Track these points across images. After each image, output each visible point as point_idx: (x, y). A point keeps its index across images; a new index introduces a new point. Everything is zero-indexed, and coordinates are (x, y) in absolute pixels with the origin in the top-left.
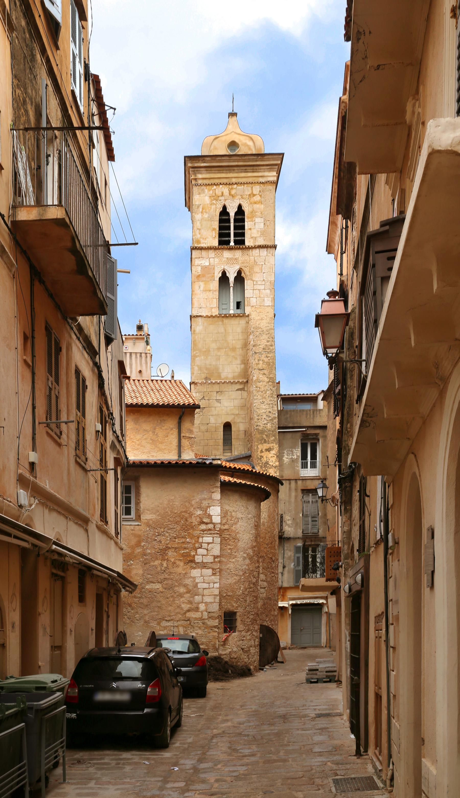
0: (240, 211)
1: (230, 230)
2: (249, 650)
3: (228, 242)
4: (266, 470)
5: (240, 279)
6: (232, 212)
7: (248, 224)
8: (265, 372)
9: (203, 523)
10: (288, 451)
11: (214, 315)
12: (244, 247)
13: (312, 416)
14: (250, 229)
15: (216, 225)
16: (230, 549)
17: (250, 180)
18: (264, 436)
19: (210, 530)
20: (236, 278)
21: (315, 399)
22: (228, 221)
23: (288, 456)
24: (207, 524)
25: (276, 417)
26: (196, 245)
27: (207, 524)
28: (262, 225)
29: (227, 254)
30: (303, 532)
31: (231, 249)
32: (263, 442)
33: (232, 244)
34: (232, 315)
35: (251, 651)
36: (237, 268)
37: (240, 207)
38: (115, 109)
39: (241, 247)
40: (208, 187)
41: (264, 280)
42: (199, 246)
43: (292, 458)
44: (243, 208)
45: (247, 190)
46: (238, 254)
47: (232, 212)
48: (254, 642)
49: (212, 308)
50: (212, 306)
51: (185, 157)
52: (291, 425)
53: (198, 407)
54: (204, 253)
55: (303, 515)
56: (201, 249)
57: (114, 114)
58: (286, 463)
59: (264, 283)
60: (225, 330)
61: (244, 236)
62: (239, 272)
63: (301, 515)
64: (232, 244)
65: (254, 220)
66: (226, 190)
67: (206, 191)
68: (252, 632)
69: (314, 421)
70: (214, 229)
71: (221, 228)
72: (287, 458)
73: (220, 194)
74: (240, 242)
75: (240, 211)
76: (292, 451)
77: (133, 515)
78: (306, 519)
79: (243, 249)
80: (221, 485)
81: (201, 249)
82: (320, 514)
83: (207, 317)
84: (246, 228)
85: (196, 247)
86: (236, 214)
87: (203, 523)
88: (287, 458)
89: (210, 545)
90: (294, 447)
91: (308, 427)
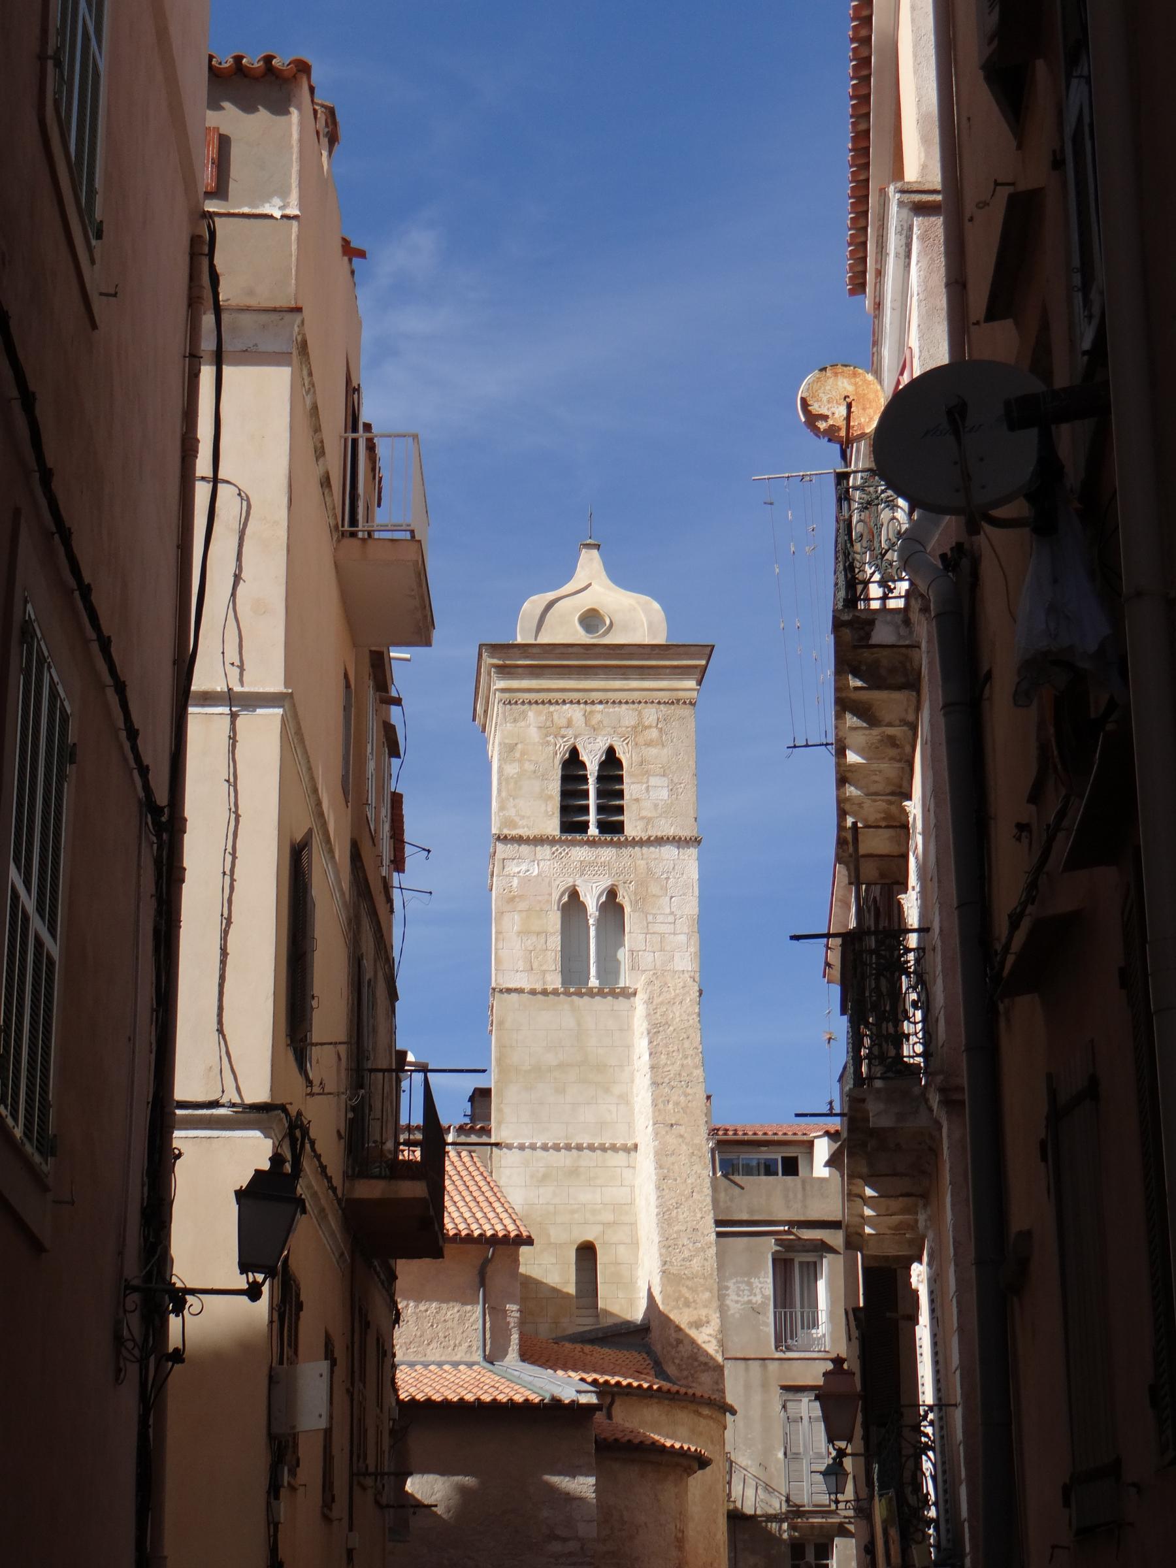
0: (611, 761)
1: (587, 798)
3: (583, 827)
4: (692, 1376)
5: (612, 904)
6: (592, 763)
7: (631, 788)
8: (682, 1130)
9: (557, 1538)
10: (737, 1282)
11: (550, 988)
12: (622, 839)
13: (800, 1196)
14: (637, 800)
15: (554, 787)
17: (636, 696)
18: (684, 1290)
19: (570, 1554)
20: (603, 908)
23: (738, 1295)
24: (565, 1540)
26: (506, 831)
27: (565, 1540)
28: (664, 794)
29: (580, 853)
31: (592, 843)
32: (681, 1303)
33: (593, 830)
34: (595, 990)
36: (605, 883)
37: (611, 751)
38: (429, 851)
40: (534, 706)
41: (672, 913)
43: (750, 1302)
45: (627, 716)
46: (607, 854)
47: (592, 763)
49: (544, 972)
50: (544, 968)
51: (481, 646)
52: (745, 1217)
53: (529, 1241)
54: (525, 849)
55: (785, 1454)
56: (520, 840)
57: (427, 858)
58: (733, 1315)
59: (671, 919)
60: (579, 1024)
62: (612, 893)
63: (781, 1455)
64: (593, 830)
66: (575, 713)
67: (531, 714)
69: (805, 1207)
70: (550, 797)
71: (565, 794)
72: (737, 1302)
73: (563, 722)
74: (612, 828)
75: (611, 761)
76: (749, 1284)
79: (619, 845)
80: (596, 1449)
81: (520, 840)
83: (533, 992)
84: (626, 796)
86: (602, 765)
87: (557, 1538)
88: (737, 1302)
90: (752, 1271)
91: (792, 1224)
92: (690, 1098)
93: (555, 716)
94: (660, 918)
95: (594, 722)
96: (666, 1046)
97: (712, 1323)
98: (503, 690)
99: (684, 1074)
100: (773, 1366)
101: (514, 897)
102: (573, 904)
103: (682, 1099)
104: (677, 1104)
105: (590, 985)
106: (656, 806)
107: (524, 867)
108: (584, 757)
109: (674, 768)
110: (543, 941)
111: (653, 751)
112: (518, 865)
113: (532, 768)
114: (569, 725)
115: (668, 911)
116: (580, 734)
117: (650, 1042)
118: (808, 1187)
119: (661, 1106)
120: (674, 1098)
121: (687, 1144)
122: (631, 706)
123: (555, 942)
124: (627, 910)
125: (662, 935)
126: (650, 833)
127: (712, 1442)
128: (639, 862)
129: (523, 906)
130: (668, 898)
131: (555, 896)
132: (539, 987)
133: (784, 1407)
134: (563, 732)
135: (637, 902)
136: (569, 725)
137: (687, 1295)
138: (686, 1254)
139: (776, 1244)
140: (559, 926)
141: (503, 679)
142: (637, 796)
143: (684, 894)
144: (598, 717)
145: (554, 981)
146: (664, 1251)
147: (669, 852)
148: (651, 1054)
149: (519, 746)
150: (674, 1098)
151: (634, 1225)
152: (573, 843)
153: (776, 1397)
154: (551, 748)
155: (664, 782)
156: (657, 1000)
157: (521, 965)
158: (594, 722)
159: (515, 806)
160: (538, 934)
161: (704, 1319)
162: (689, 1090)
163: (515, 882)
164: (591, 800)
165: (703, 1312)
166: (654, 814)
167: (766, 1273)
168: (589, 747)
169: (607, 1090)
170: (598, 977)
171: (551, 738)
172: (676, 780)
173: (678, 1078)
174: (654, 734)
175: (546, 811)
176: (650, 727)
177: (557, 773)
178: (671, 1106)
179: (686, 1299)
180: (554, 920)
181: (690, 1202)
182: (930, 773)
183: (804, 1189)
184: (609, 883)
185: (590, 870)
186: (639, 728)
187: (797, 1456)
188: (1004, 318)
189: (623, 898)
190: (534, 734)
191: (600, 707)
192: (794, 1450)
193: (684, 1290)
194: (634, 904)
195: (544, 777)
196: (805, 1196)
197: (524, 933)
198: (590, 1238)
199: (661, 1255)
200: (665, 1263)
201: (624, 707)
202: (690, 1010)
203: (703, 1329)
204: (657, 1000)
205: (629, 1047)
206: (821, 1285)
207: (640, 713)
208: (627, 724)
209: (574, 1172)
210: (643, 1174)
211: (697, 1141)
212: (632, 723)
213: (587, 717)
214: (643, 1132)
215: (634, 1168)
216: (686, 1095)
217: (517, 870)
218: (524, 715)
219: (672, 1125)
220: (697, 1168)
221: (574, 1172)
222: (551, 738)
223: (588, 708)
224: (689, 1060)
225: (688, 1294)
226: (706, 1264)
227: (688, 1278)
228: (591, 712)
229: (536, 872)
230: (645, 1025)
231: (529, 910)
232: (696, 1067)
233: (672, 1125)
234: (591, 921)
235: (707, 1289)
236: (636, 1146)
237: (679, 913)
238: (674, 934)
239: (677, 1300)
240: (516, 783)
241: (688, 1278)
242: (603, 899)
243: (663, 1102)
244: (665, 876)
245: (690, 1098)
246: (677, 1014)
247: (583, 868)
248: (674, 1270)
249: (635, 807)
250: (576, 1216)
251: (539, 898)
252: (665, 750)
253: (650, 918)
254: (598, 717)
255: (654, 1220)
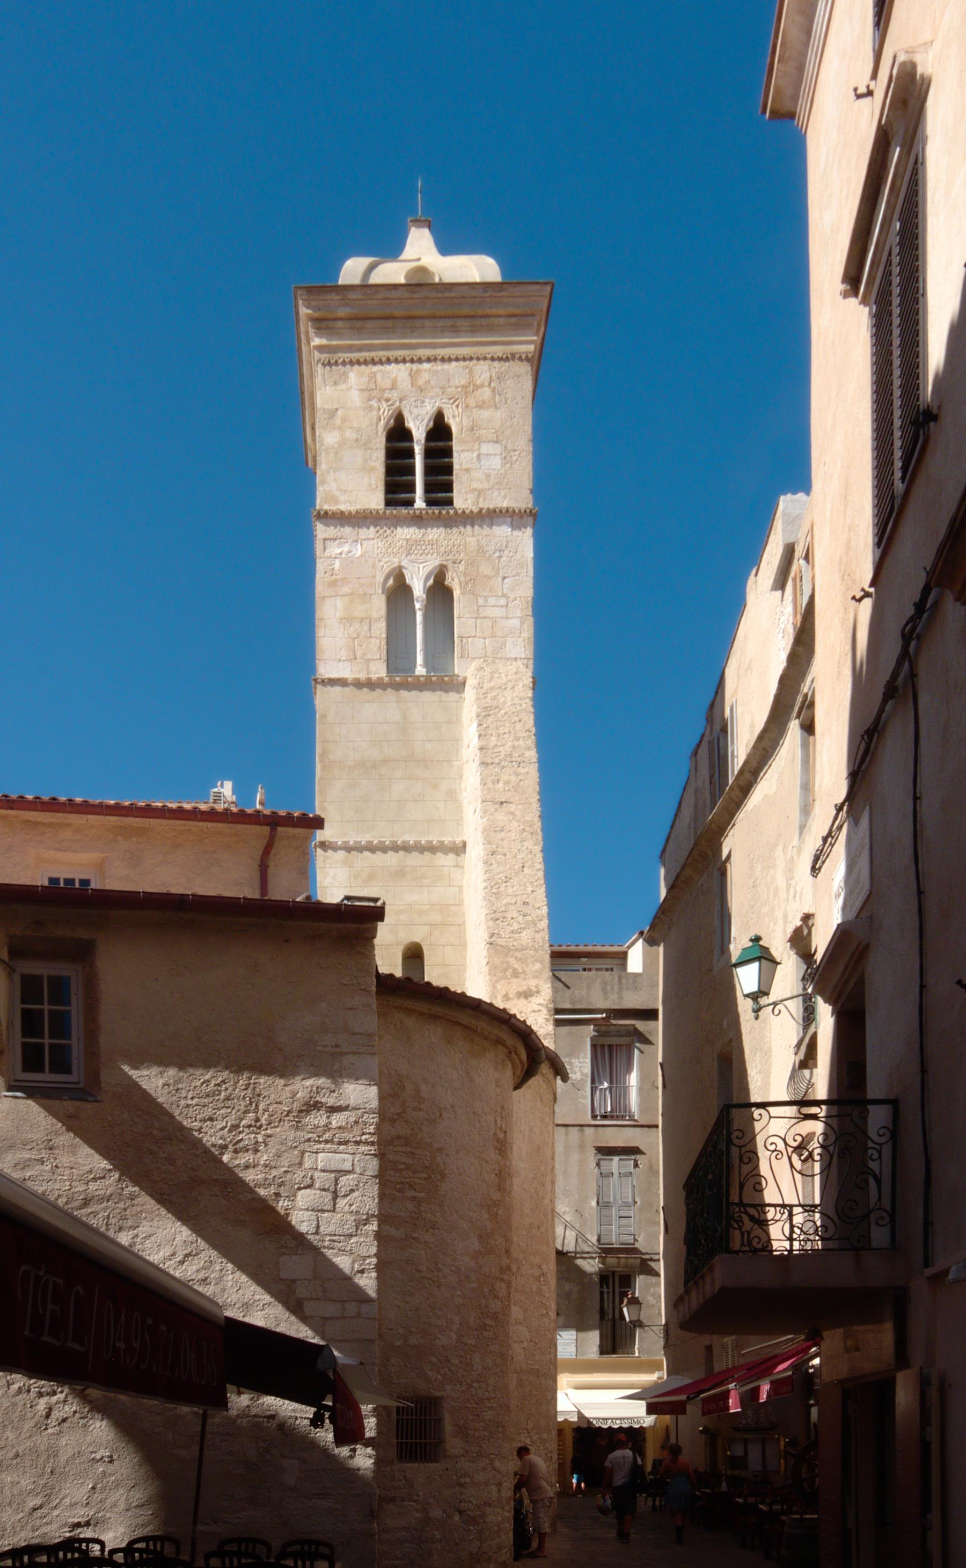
0: (440, 431)
1: (414, 491)
2: (483, 1516)
5: (440, 591)
6: (419, 430)
7: (461, 459)
8: (512, 808)
11: (374, 677)
13: (616, 988)
14: (467, 470)
16: (414, 1198)
18: (512, 961)
21: (621, 956)
22: (410, 454)
25: (542, 916)
28: (497, 463)
30: (599, 1240)
32: (509, 973)
33: (420, 503)
35: (490, 1518)
36: (433, 563)
39: (444, 512)
40: (356, 367)
41: (504, 595)
42: (334, 508)
44: (446, 419)
46: (435, 533)
47: (419, 430)
48: (499, 1491)
50: (368, 656)
55: (598, 1203)
59: (503, 601)
61: (451, 491)
63: (594, 1203)
64: (420, 503)
65: (476, 447)
66: (399, 372)
68: (492, 1461)
70: (374, 469)
73: (387, 384)
75: (440, 431)
77: (77, 1075)
78: (605, 1212)
82: (639, 1203)
83: (358, 684)
85: (326, 513)
89: (343, 1180)
92: (521, 777)
93: (379, 377)
94: (492, 601)
95: (421, 382)
96: (497, 728)
97: (543, 993)
98: (320, 348)
99: (515, 755)
100: (589, 1131)
101: (336, 581)
102: (399, 592)
103: (513, 778)
104: (507, 783)
105: (417, 673)
106: (488, 476)
107: (346, 548)
108: (410, 424)
109: (508, 432)
110: (366, 627)
111: (486, 414)
112: (340, 545)
113: (354, 436)
114: (394, 387)
115: (500, 594)
116: (405, 396)
117: (480, 725)
118: (624, 981)
119: (490, 785)
120: (505, 777)
121: (518, 821)
122: (461, 363)
123: (380, 628)
124: (456, 593)
125: (494, 620)
126: (481, 505)
127: (542, 1100)
128: (469, 539)
129: (346, 589)
130: (500, 579)
131: (380, 578)
132: (362, 676)
133: (598, 1165)
134: (386, 395)
135: (467, 583)
136: (394, 387)
137: (516, 966)
138: (516, 926)
139: (594, 1030)
140: (383, 612)
141: (321, 337)
142: (468, 466)
143: (517, 574)
144: (426, 376)
145: (379, 671)
146: (491, 923)
147: (503, 531)
148: (480, 736)
149: (340, 412)
150: (505, 777)
151: (462, 925)
152: (397, 522)
153: (591, 1157)
154: (374, 413)
155: (497, 449)
156: (487, 685)
157: (344, 654)
158: (421, 382)
159: (335, 480)
160: (362, 620)
161: (534, 989)
162: (521, 770)
163: (337, 564)
164: (418, 469)
165: (533, 983)
166: (486, 486)
167: (586, 1054)
168: (415, 411)
169: (435, 787)
170: (426, 664)
171: (374, 403)
172: (510, 447)
173: (509, 759)
174: (486, 393)
175: (370, 485)
176: (482, 386)
177: (380, 443)
178: (501, 785)
179: (515, 969)
180: (378, 605)
181: (521, 876)
182: (890, 158)
183: (620, 982)
184: (437, 563)
185: (416, 552)
186: (470, 388)
187: (607, 1205)
188: (555, 1381)
189: (453, 581)
190: (355, 398)
191: (426, 366)
192: (606, 1200)
193: (512, 961)
194: (463, 586)
195: (366, 446)
196: (620, 988)
197: (348, 620)
198: (416, 939)
199: (488, 928)
200: (492, 935)
201: (454, 364)
202: (523, 694)
203: (533, 999)
204: (487, 685)
205: (457, 740)
206: (633, 1079)
207: (471, 371)
208: (457, 383)
209: (400, 873)
210: (472, 875)
211: (528, 818)
212: (463, 382)
213: (413, 376)
214: (471, 827)
215: (462, 867)
216: (517, 775)
217: (338, 551)
218: (345, 376)
219: (502, 803)
220: (529, 844)
221: (400, 873)
222: (374, 403)
223: (415, 366)
224: (521, 742)
225: (516, 966)
226: (537, 936)
227: (517, 950)
228: (418, 371)
229: (359, 553)
230: (475, 709)
231: (352, 594)
232: (529, 749)
233: (502, 803)
234: (418, 606)
235: (537, 961)
236: (464, 844)
237: (512, 596)
238: (507, 618)
239: (504, 971)
240: (336, 453)
241: (517, 950)
242: (431, 581)
243: (493, 781)
244: (497, 554)
245: (521, 777)
246: (509, 699)
247: (410, 547)
248: (500, 941)
249: (465, 478)
250: (402, 917)
251: (362, 581)
252: (499, 413)
253: (481, 601)
254: (426, 376)
255: (481, 894)
